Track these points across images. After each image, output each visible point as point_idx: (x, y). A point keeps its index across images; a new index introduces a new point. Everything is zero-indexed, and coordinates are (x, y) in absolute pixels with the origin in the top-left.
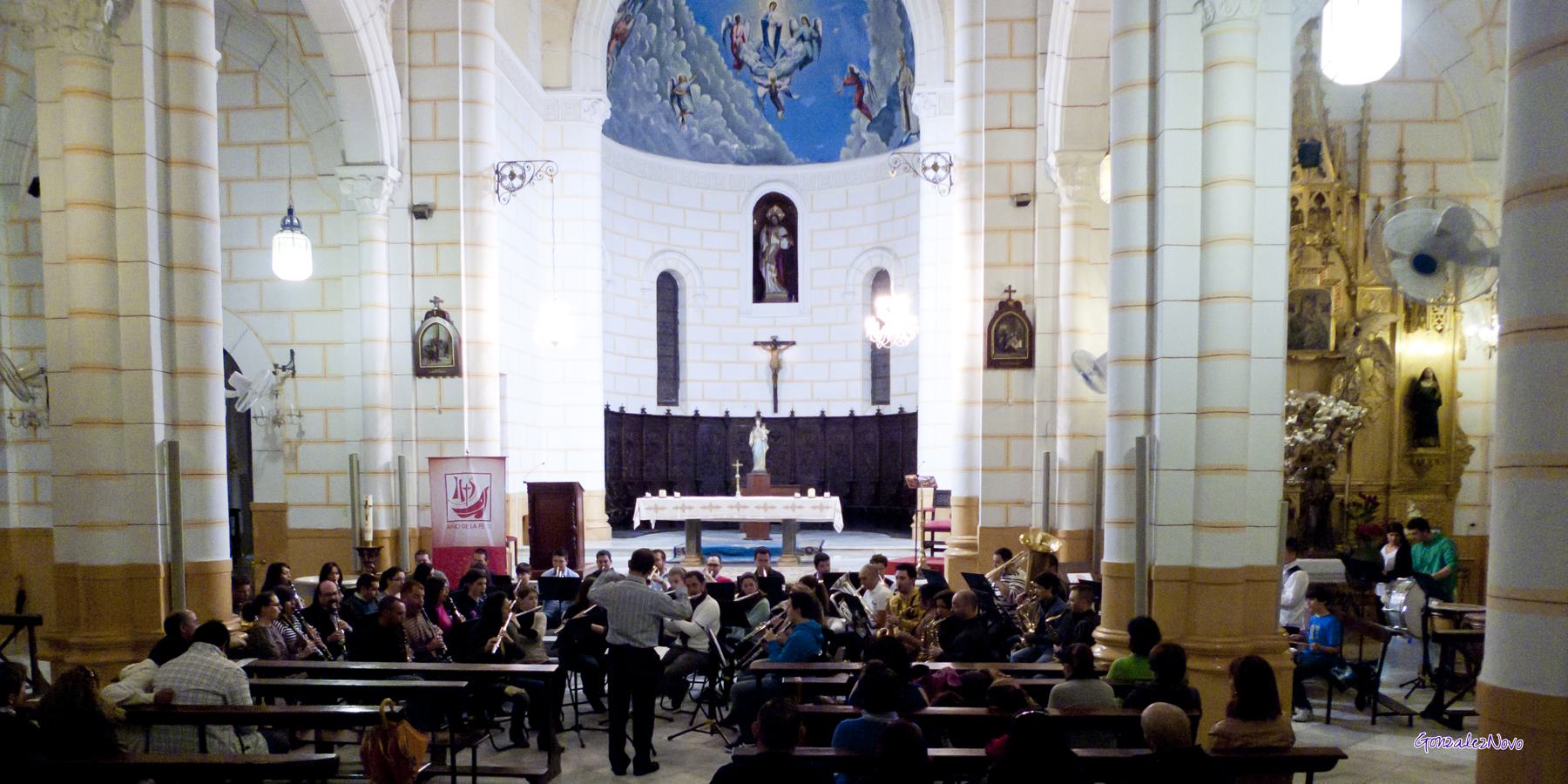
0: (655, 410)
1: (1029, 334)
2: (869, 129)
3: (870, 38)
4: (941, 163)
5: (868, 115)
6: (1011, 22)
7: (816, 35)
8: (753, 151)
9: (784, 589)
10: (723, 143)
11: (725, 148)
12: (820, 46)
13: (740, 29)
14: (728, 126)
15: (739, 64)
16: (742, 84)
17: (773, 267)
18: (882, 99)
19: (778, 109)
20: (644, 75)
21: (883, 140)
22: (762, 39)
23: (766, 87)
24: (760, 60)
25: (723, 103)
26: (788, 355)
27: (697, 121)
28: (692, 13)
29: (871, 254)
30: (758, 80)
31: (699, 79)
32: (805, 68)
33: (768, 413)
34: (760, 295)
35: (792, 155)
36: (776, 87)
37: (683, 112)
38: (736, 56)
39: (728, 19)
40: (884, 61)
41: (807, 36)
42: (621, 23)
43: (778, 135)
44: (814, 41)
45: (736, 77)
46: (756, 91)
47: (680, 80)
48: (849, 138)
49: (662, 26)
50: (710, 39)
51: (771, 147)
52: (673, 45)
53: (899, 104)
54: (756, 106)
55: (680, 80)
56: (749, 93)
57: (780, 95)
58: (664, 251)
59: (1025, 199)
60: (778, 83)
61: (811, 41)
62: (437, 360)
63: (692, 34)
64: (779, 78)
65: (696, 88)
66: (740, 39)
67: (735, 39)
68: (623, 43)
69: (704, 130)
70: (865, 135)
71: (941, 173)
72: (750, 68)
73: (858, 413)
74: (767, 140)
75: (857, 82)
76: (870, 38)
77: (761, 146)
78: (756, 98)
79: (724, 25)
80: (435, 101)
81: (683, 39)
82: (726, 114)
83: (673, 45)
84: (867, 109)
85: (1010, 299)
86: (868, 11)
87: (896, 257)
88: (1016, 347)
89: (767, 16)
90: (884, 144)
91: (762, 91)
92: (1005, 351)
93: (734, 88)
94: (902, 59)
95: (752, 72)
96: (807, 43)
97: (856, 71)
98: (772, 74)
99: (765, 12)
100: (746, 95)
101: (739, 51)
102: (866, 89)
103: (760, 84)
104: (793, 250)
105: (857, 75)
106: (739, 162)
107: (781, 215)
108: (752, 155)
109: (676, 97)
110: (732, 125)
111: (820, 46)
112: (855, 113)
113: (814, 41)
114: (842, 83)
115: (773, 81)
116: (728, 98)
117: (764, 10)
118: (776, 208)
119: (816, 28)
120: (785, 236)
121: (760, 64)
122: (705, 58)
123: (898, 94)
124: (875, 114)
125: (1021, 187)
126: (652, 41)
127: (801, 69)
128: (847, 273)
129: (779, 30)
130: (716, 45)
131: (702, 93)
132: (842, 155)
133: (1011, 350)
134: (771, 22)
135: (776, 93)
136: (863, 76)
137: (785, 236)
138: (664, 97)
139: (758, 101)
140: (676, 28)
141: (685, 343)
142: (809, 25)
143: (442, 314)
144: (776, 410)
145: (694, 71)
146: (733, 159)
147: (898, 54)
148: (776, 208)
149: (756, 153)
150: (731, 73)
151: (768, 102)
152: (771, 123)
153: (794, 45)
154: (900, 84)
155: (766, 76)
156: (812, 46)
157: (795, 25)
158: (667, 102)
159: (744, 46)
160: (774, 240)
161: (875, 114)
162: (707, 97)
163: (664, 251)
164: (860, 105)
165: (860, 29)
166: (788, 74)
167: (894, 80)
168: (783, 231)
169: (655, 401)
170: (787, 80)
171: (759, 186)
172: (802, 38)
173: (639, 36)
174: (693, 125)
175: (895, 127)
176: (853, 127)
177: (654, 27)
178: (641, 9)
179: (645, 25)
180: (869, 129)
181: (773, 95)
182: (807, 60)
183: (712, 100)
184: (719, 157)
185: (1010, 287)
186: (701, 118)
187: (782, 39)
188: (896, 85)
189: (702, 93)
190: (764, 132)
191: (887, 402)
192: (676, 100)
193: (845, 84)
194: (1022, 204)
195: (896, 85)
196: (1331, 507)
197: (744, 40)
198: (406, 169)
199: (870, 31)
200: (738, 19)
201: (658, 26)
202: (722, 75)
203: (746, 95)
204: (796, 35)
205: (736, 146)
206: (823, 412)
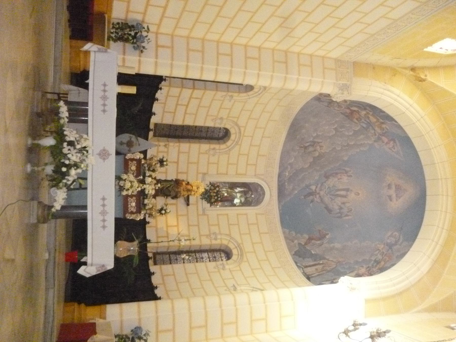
0: (154, 120)
5: (306, 244)
7: (343, 216)
8: (285, 183)
9: (226, 194)
23: (315, 190)
24: (329, 187)
30: (319, 185)
36: (316, 195)
39: (350, 171)
42: (358, 116)
44: (340, 215)
48: (294, 233)
53: (315, 260)
55: (321, 147)
57: (311, 197)
60: (318, 196)
61: (340, 213)
64: (320, 196)
66: (339, 177)
68: (347, 116)
72: (325, 182)
77: (287, 187)
78: (310, 185)
83: (340, 143)
84: (309, 243)
90: (293, 253)
97: (327, 237)
98: (322, 193)
103: (317, 187)
105: (325, 237)
106: (279, 176)
112: (306, 236)
113: (340, 215)
114: (320, 229)
115: (319, 194)
119: (347, 215)
123: (320, 260)
124: (308, 248)
127: (325, 207)
128: (226, 235)
129: (345, 196)
134: (349, 193)
135: (313, 195)
136: (325, 241)
138: (314, 138)
139: (308, 186)
140: (348, 145)
142: (348, 212)
154: (326, 261)
155: (321, 190)
157: (347, 205)
158: (311, 139)
159: (336, 179)
162: (312, 160)
164: (310, 239)
166: (322, 200)
167: (327, 258)
170: (319, 200)
172: (341, 208)
173: (348, 125)
175: (304, 258)
176: (299, 235)
180: (300, 244)
182: (329, 211)
184: (283, 166)
187: (339, 198)
188: (324, 258)
190: (293, 189)
191: (155, 264)
193: (320, 231)
195: (324, 258)
197: (339, 179)
204: (342, 206)
205: (287, 174)
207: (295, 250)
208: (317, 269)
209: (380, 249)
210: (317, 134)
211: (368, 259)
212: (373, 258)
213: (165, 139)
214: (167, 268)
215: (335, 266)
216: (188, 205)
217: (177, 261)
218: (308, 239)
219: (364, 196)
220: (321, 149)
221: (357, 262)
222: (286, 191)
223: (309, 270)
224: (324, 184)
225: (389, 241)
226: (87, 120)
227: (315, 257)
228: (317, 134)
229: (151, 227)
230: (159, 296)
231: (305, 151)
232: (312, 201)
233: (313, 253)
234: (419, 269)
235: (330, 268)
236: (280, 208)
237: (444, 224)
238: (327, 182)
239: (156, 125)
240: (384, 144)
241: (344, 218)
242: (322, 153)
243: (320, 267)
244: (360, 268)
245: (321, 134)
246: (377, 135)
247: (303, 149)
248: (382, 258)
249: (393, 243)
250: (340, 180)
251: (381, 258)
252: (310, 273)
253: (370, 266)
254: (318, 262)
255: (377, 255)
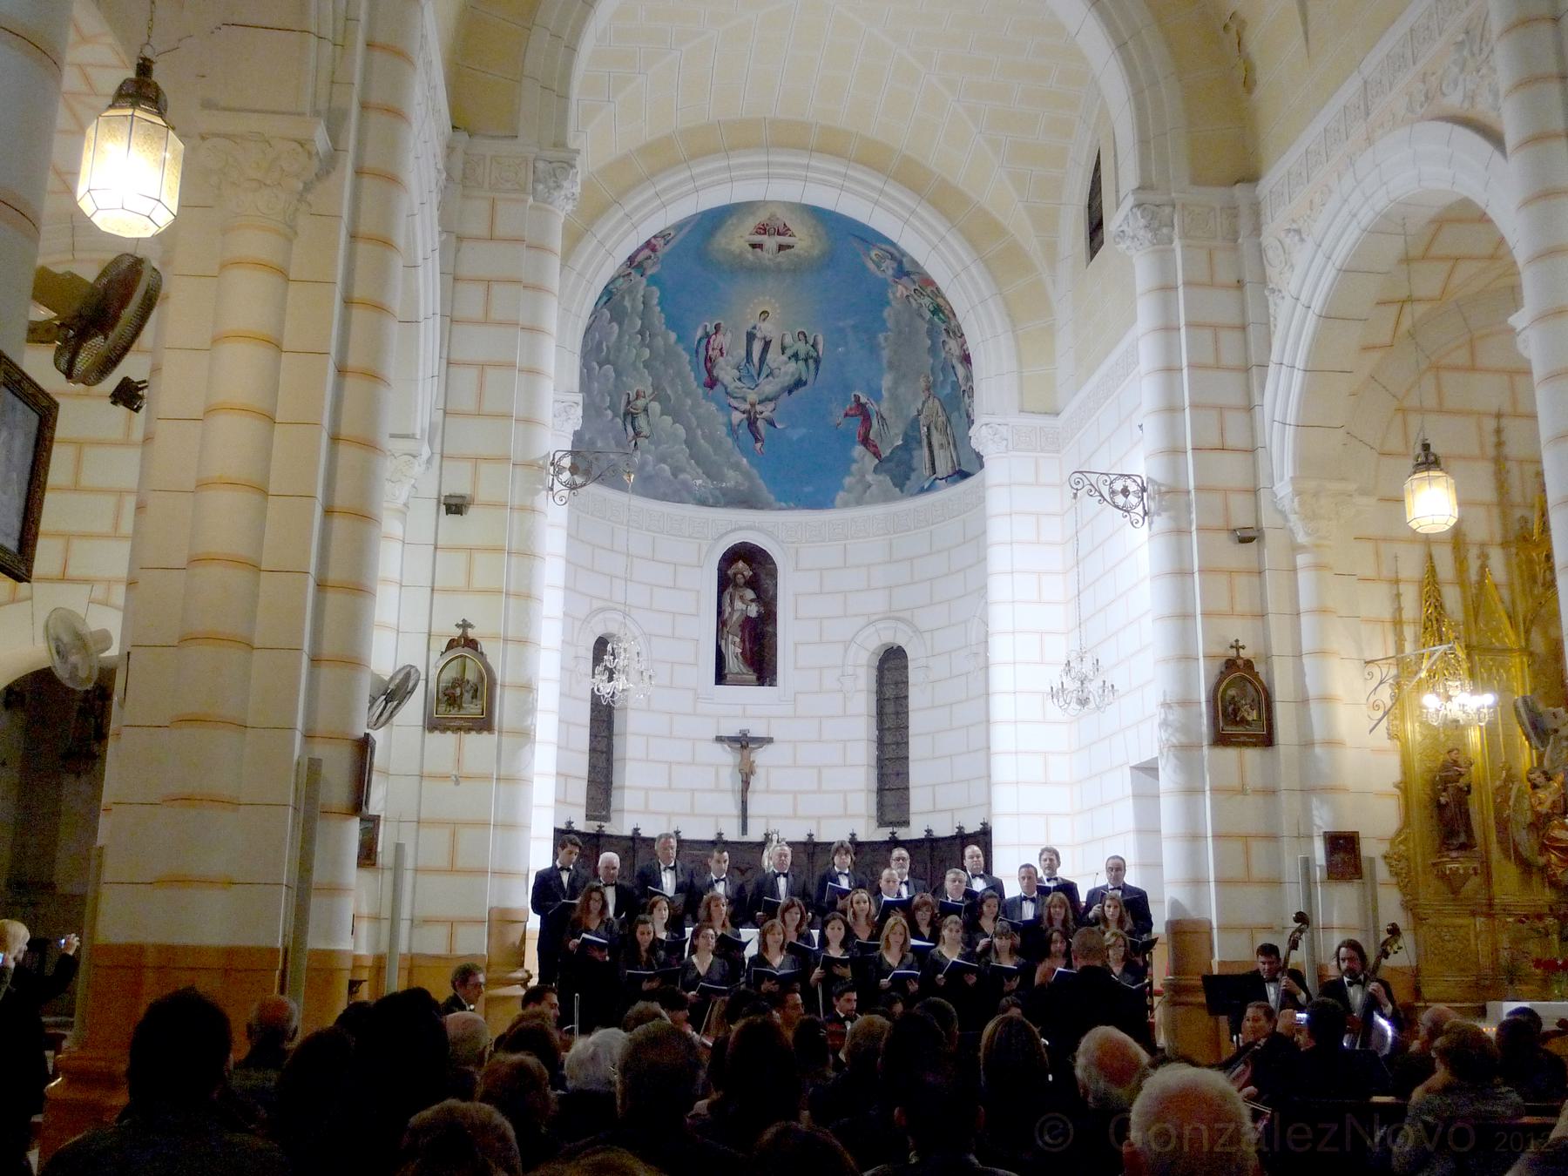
1: (1265, 702)
2: (876, 470)
3: (885, 361)
4: (1133, 487)
5: (877, 454)
6: (1215, 328)
7: (815, 354)
10: (682, 476)
11: (684, 483)
12: (817, 369)
13: (719, 340)
14: (692, 456)
15: (712, 383)
16: (713, 407)
17: (737, 640)
18: (897, 435)
19: (757, 440)
20: (596, 385)
21: (895, 485)
22: (744, 353)
23: (744, 413)
24: (740, 379)
25: (688, 429)
26: (761, 756)
27: (653, 447)
28: (663, 315)
29: (881, 625)
30: (735, 403)
31: (659, 395)
32: (795, 393)
33: (732, 834)
34: (720, 678)
35: (772, 498)
37: (637, 434)
38: (709, 372)
40: (902, 390)
41: (802, 355)
43: (754, 472)
44: (811, 362)
45: (706, 397)
46: (729, 416)
47: (638, 396)
48: (847, 481)
49: (625, 327)
50: (680, 349)
51: (745, 486)
52: (635, 351)
53: (920, 442)
54: (728, 435)
55: (638, 396)
56: (722, 418)
57: (761, 424)
58: (602, 610)
59: (1251, 534)
60: (759, 408)
61: (806, 360)
62: (460, 707)
63: (659, 341)
64: (761, 402)
65: (655, 407)
67: (710, 352)
69: (662, 459)
70: (870, 478)
71: (1133, 499)
73: (861, 838)
74: (740, 478)
75: (862, 412)
76: (885, 361)
77: (731, 484)
79: (700, 333)
80: (483, 366)
81: (648, 346)
82: (690, 442)
84: (875, 446)
85: (1238, 656)
86: (886, 330)
87: (916, 631)
88: (1250, 718)
89: (754, 328)
91: (737, 417)
92: (1236, 723)
93: (702, 411)
94: (928, 389)
95: (727, 393)
96: (801, 363)
97: (863, 400)
98: (752, 396)
99: (752, 323)
100: (715, 418)
101: (713, 366)
102: (875, 422)
104: (769, 615)
106: (702, 502)
107: (748, 573)
108: (717, 493)
109: (630, 416)
110: (696, 456)
111: (817, 369)
112: (859, 450)
113: (811, 362)
115: (753, 405)
116: (694, 422)
117: (752, 320)
118: (741, 564)
120: (752, 601)
121: (739, 384)
122: (671, 371)
124: (886, 452)
125: (1242, 519)
126: (610, 345)
129: (767, 344)
130: (686, 357)
131: (663, 414)
132: (838, 500)
133: (1244, 721)
134: (759, 335)
136: (872, 407)
137: (752, 601)
138: (616, 415)
139: (732, 430)
140: (641, 333)
141: (624, 734)
143: (472, 644)
144: (744, 829)
145: (656, 387)
146: (694, 499)
147: (922, 383)
148: (741, 564)
149: (724, 492)
150: (700, 391)
151: (743, 431)
152: (747, 457)
153: (786, 363)
156: (807, 366)
157: (788, 340)
158: (619, 421)
160: (739, 605)
161: (886, 452)
162: (668, 419)
163: (602, 610)
164: (865, 441)
165: (874, 350)
168: (750, 594)
169: (582, 812)
170: (771, 406)
171: (726, 533)
172: (795, 356)
173: (597, 336)
174: (648, 452)
176: (854, 467)
177: (615, 326)
178: (606, 303)
179: (605, 324)
180: (876, 470)
181: (752, 423)
182: (799, 383)
183: (674, 422)
184: (679, 494)
185: (1237, 641)
186: (657, 443)
187: (770, 356)
188: (916, 420)
189: (663, 414)
190: (736, 467)
191: (906, 823)
192: (629, 419)
193: (846, 415)
194: (1245, 540)
195: (916, 420)
196: (1093, 1030)
197: (722, 354)
198: (437, 449)
199: (886, 354)
200: (717, 327)
201: (620, 327)
202: (688, 394)
203: (715, 418)
204: (789, 352)
205: (699, 482)
206: (810, 836)
207: (891, 484)
208: (942, 446)
209: (905, 293)
210: (609, 407)
211: (927, 326)
212: (928, 315)
213: (614, 793)
214: (918, 799)
215: (936, 401)
216: (769, 740)
217: (902, 774)
218: (865, 445)
219: (777, 316)
220: (644, 397)
221: (933, 350)
222: (742, 488)
223: (943, 467)
224: (729, 390)
225: (890, 272)
226: (72, 1023)
227: (911, 441)
228: (609, 407)
229: (818, 830)
230: (978, 827)
231: (646, 437)
232: (771, 423)
233: (900, 442)
234: (966, 268)
235: (940, 414)
236: (783, 504)
237: (873, 188)
238: (725, 383)
239: (589, 817)
240: (652, 255)
241: (821, 353)
242: (653, 393)
243: (937, 439)
244: (947, 349)
245: (608, 399)
246: (629, 270)
247: (640, 441)
248: (929, 296)
249: (895, 265)
250: (725, 352)
251: (930, 299)
252: (950, 465)
253: (944, 326)
254: (924, 438)
255: (921, 304)
